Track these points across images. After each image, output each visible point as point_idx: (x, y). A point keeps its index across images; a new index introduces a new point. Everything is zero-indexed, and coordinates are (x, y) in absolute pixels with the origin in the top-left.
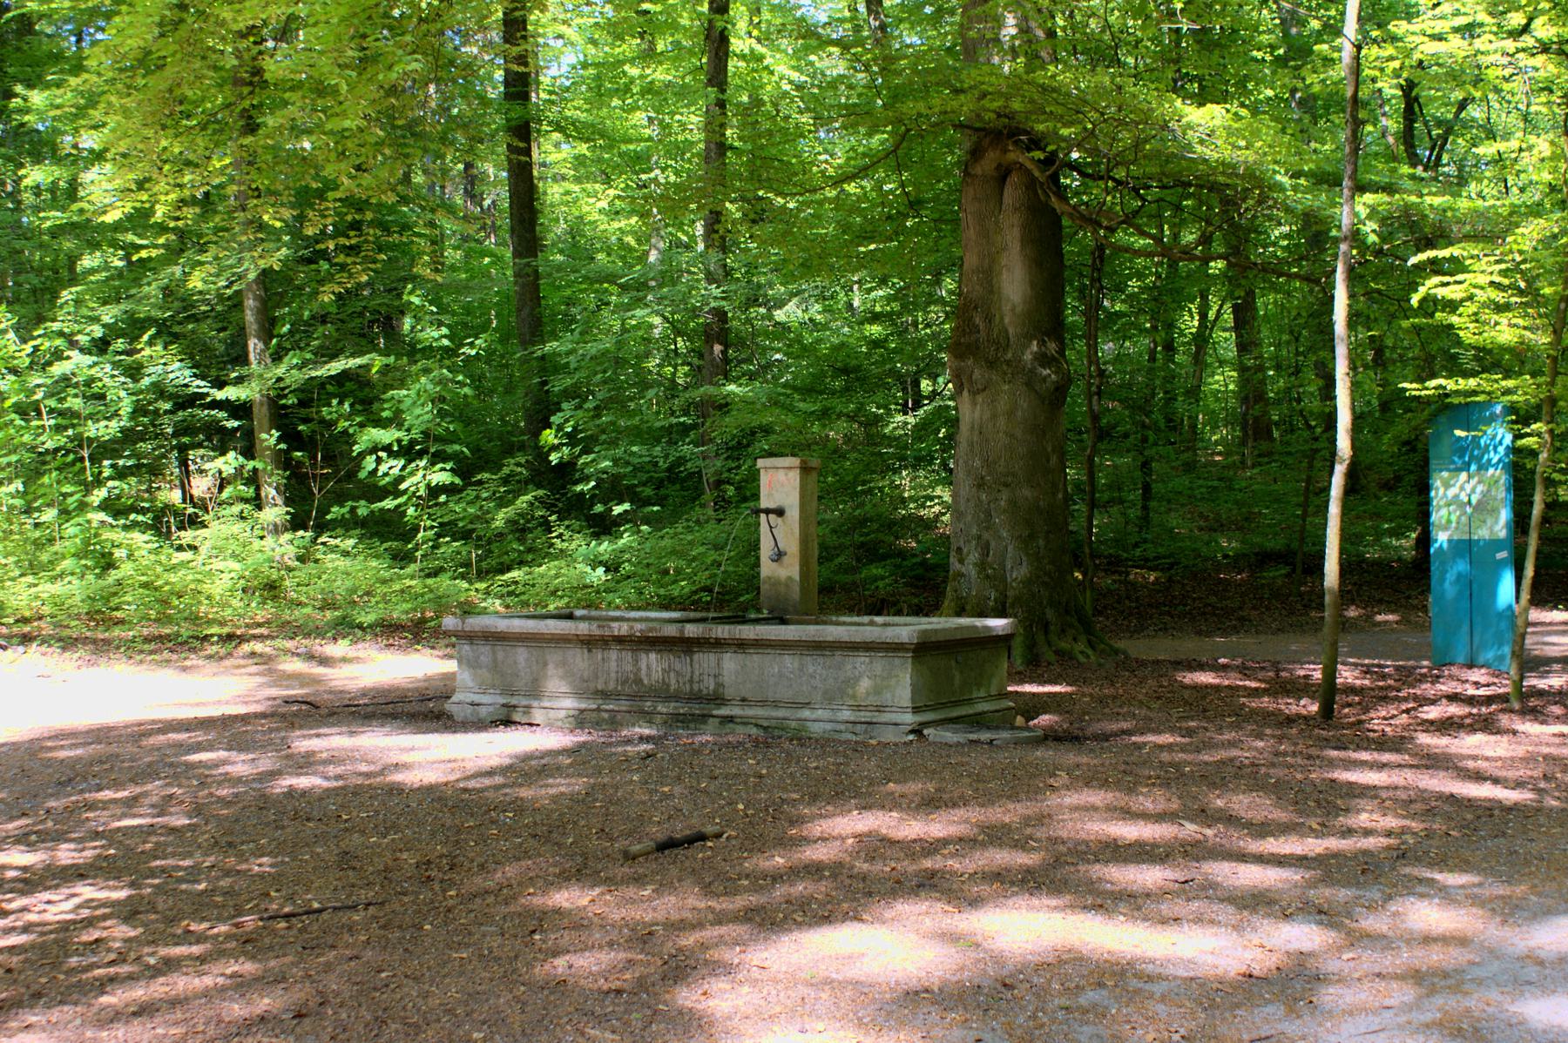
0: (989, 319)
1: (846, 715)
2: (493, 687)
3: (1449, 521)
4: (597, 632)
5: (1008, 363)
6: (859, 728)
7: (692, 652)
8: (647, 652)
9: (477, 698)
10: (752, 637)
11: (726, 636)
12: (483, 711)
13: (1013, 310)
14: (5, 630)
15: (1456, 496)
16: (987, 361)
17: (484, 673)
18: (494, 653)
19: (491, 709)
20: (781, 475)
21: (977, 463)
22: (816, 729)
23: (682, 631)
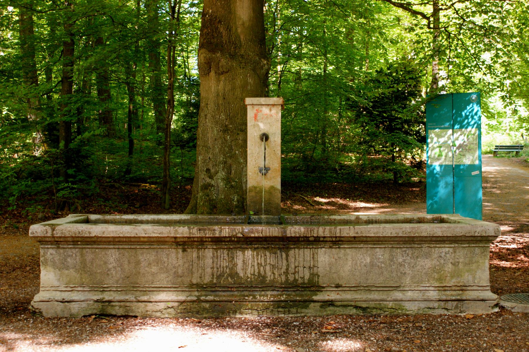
0: (229, 29)
1: (433, 294)
2: (82, 285)
3: (440, 155)
5: (242, 56)
6: (449, 305)
7: (288, 249)
8: (243, 250)
9: (67, 296)
10: (352, 234)
11: (327, 234)
12: (75, 308)
13: (243, 24)
14: (528, 294)
15: (446, 142)
16: (230, 55)
18: (82, 255)
19: (84, 305)
20: (265, 110)
21: (223, 116)
22: (412, 308)
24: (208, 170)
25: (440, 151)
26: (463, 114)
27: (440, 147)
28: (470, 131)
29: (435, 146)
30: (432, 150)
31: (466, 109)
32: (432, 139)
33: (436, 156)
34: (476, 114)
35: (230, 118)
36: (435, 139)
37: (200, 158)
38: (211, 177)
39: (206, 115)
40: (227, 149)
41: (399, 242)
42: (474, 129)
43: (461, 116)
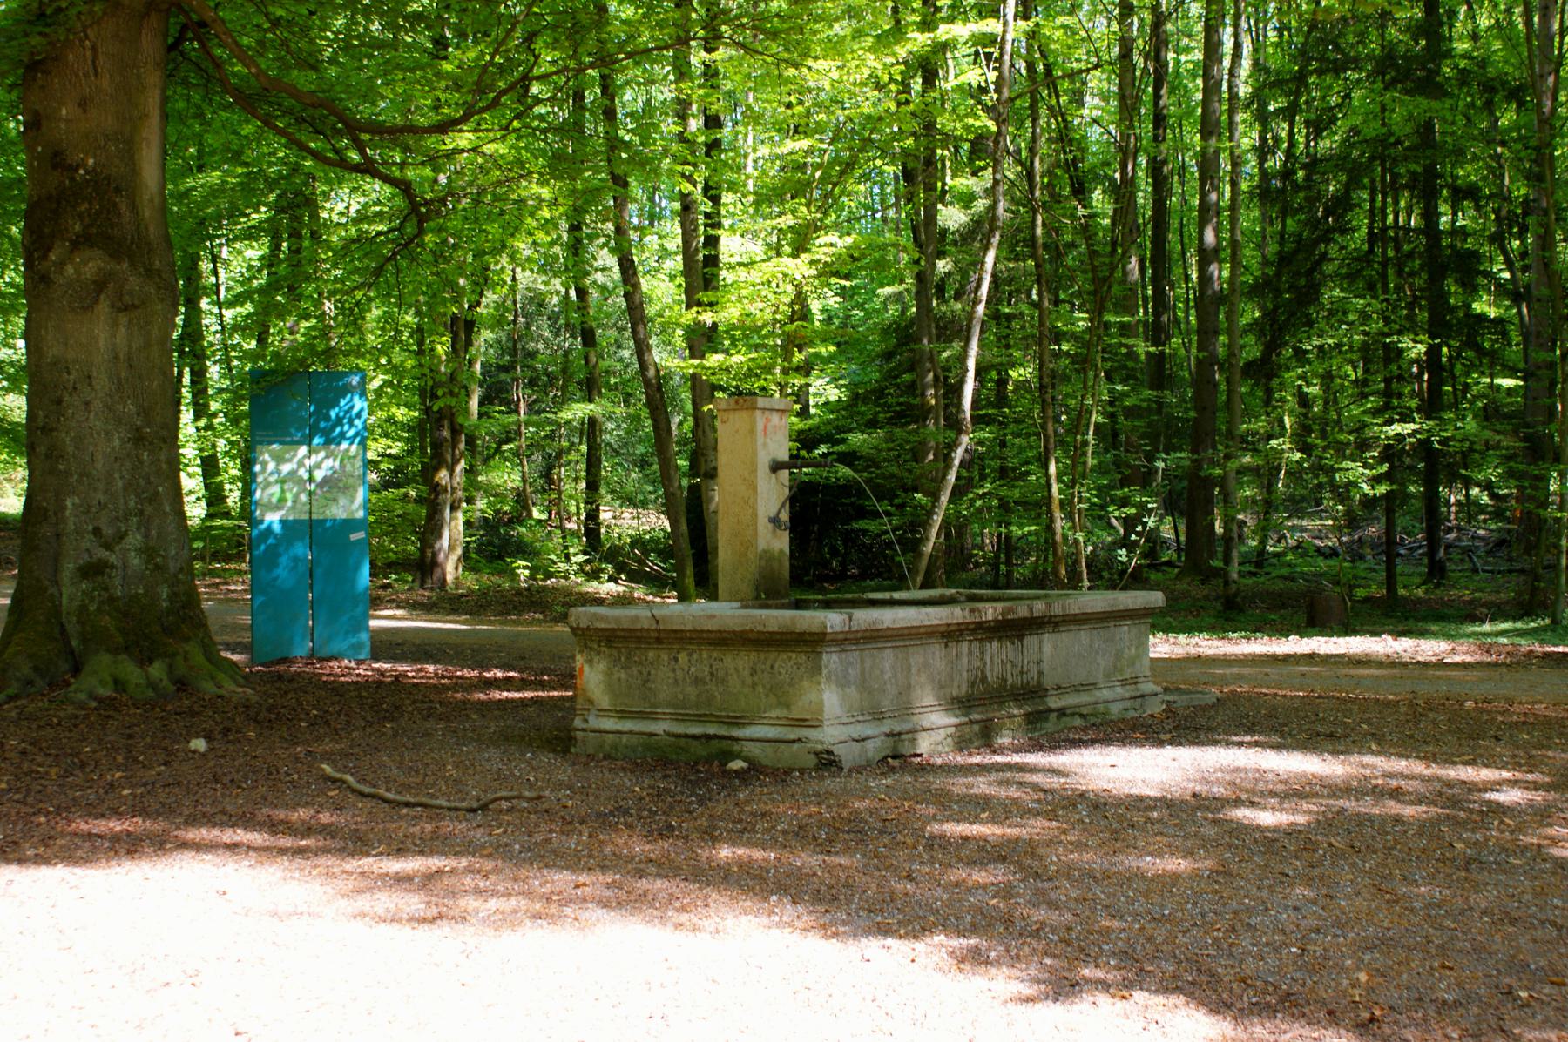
3: (282, 500)
4: (969, 620)
7: (1021, 638)
13: (151, 200)
15: (293, 473)
17: (852, 691)
23: (1031, 609)
24: (97, 531)
25: (283, 491)
26: (333, 414)
27: (283, 482)
28: (347, 450)
29: (272, 479)
30: (263, 490)
31: (337, 404)
32: (264, 464)
33: (274, 500)
34: (359, 416)
35: (145, 412)
36: (271, 466)
37: (69, 503)
38: (108, 547)
39: (87, 403)
40: (142, 482)
41: (857, 641)
42: (354, 447)
43: (328, 418)
